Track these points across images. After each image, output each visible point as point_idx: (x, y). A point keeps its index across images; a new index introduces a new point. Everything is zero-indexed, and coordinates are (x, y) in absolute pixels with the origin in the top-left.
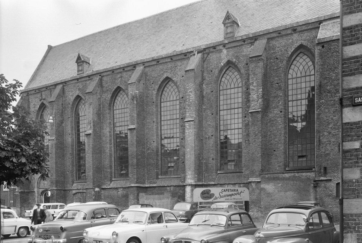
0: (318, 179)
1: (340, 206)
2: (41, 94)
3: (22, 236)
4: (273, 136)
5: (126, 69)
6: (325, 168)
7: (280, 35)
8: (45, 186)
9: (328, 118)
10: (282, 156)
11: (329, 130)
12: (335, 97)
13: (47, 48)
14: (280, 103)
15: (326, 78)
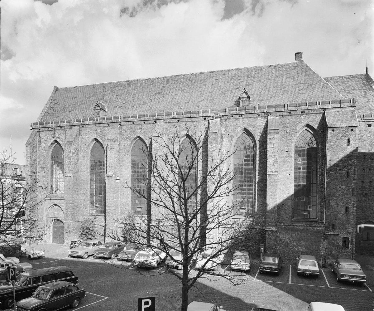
0: (327, 233)
1: (202, 179)
2: (55, 132)
3: (75, 306)
4: (282, 193)
5: (146, 122)
6: (333, 225)
7: (290, 114)
8: (54, 216)
9: (336, 186)
10: (289, 209)
11: (338, 195)
12: (343, 171)
13: (53, 89)
14: (289, 168)
15: (336, 155)
